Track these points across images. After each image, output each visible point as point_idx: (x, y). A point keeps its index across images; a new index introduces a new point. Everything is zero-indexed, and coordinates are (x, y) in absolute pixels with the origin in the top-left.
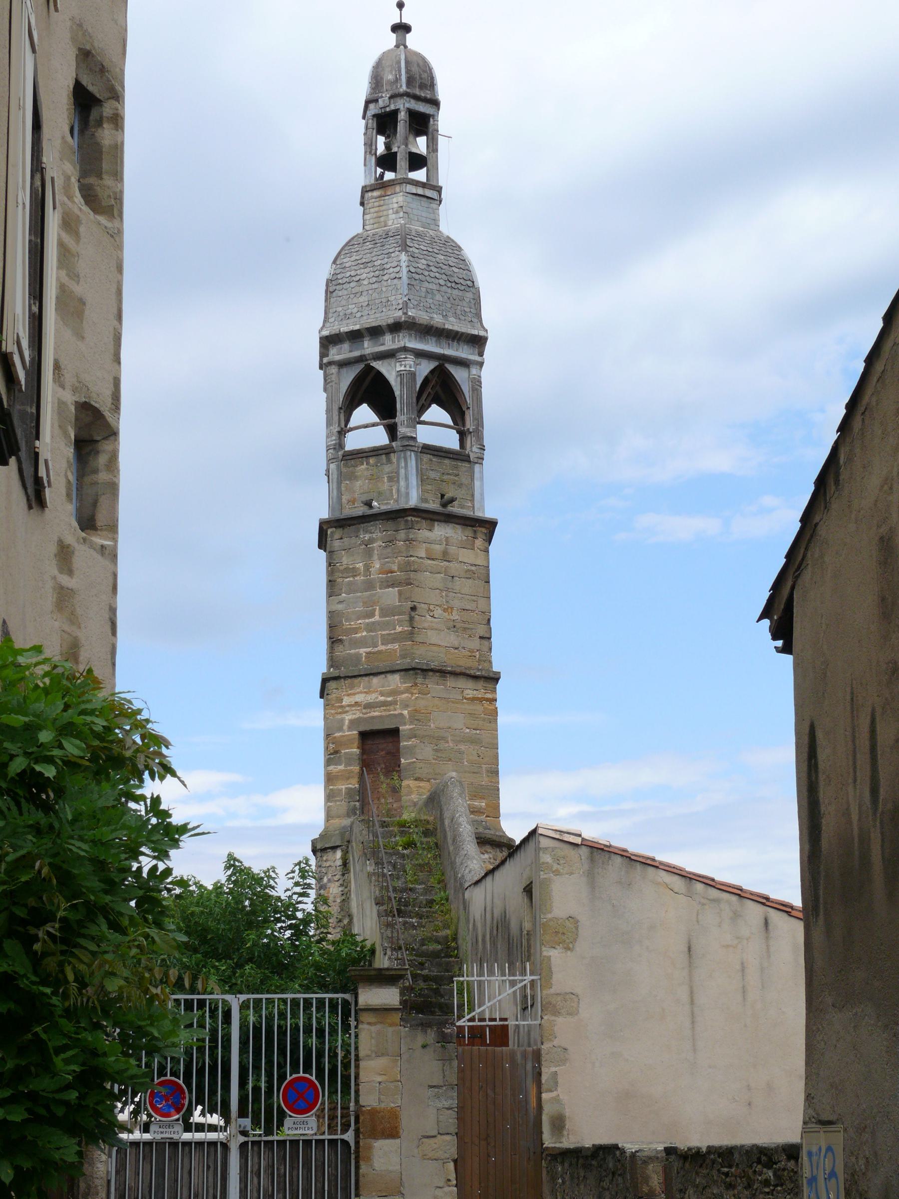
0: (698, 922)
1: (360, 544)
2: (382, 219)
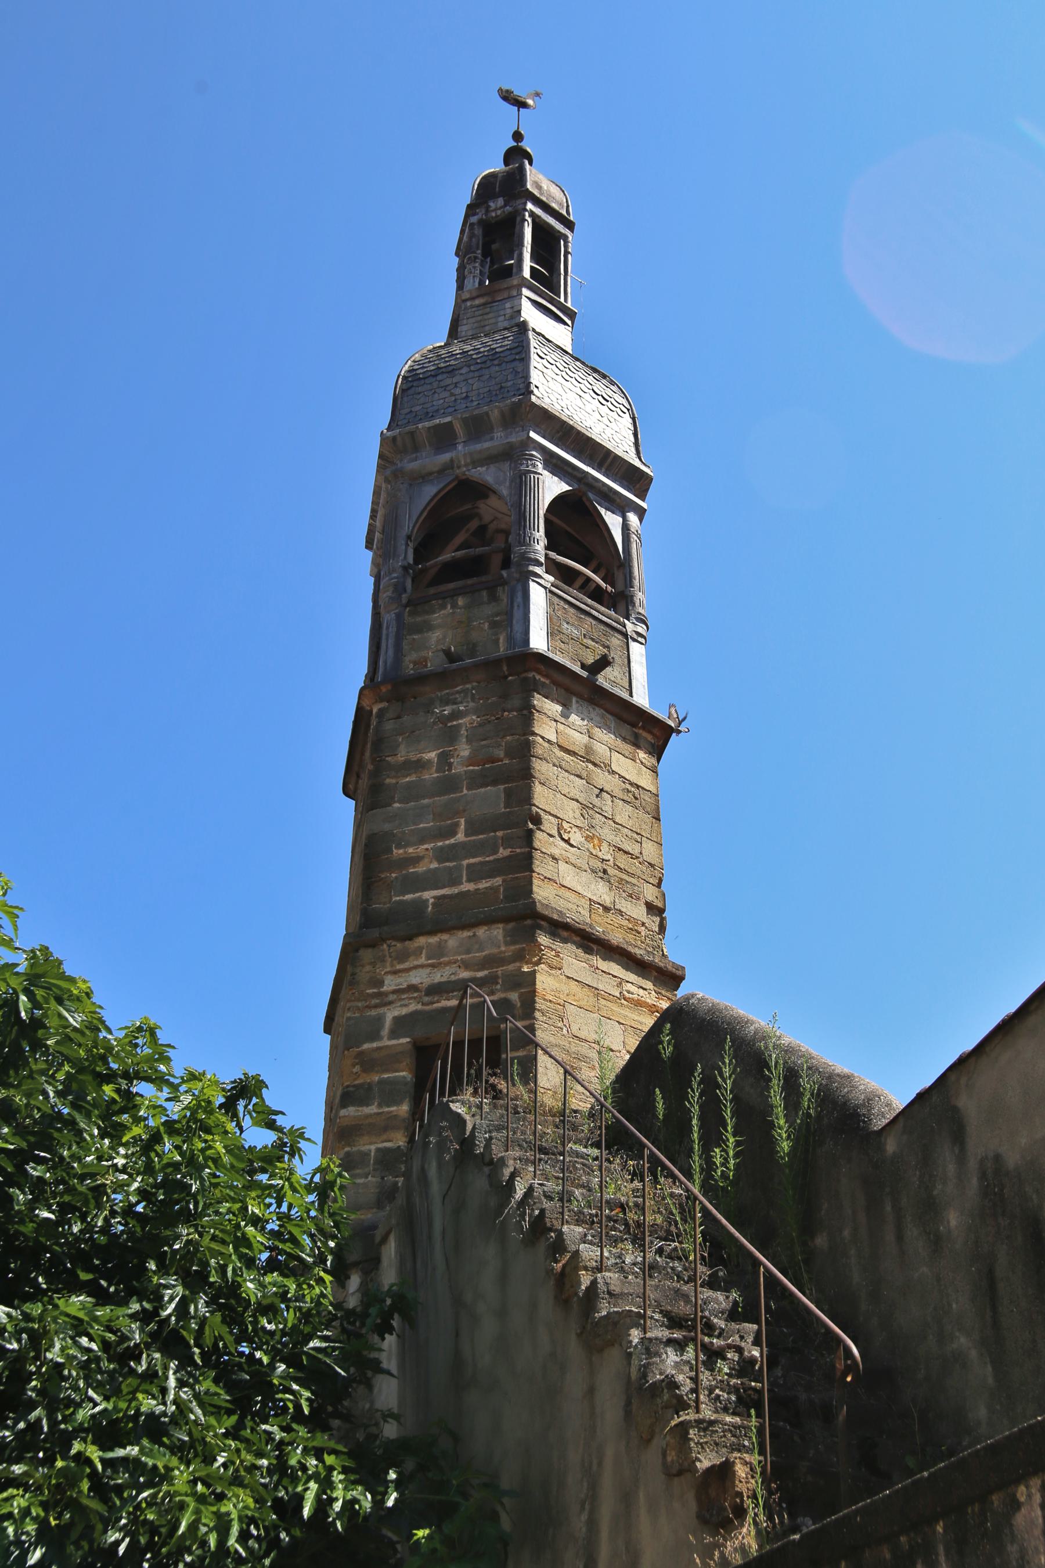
1: (434, 723)
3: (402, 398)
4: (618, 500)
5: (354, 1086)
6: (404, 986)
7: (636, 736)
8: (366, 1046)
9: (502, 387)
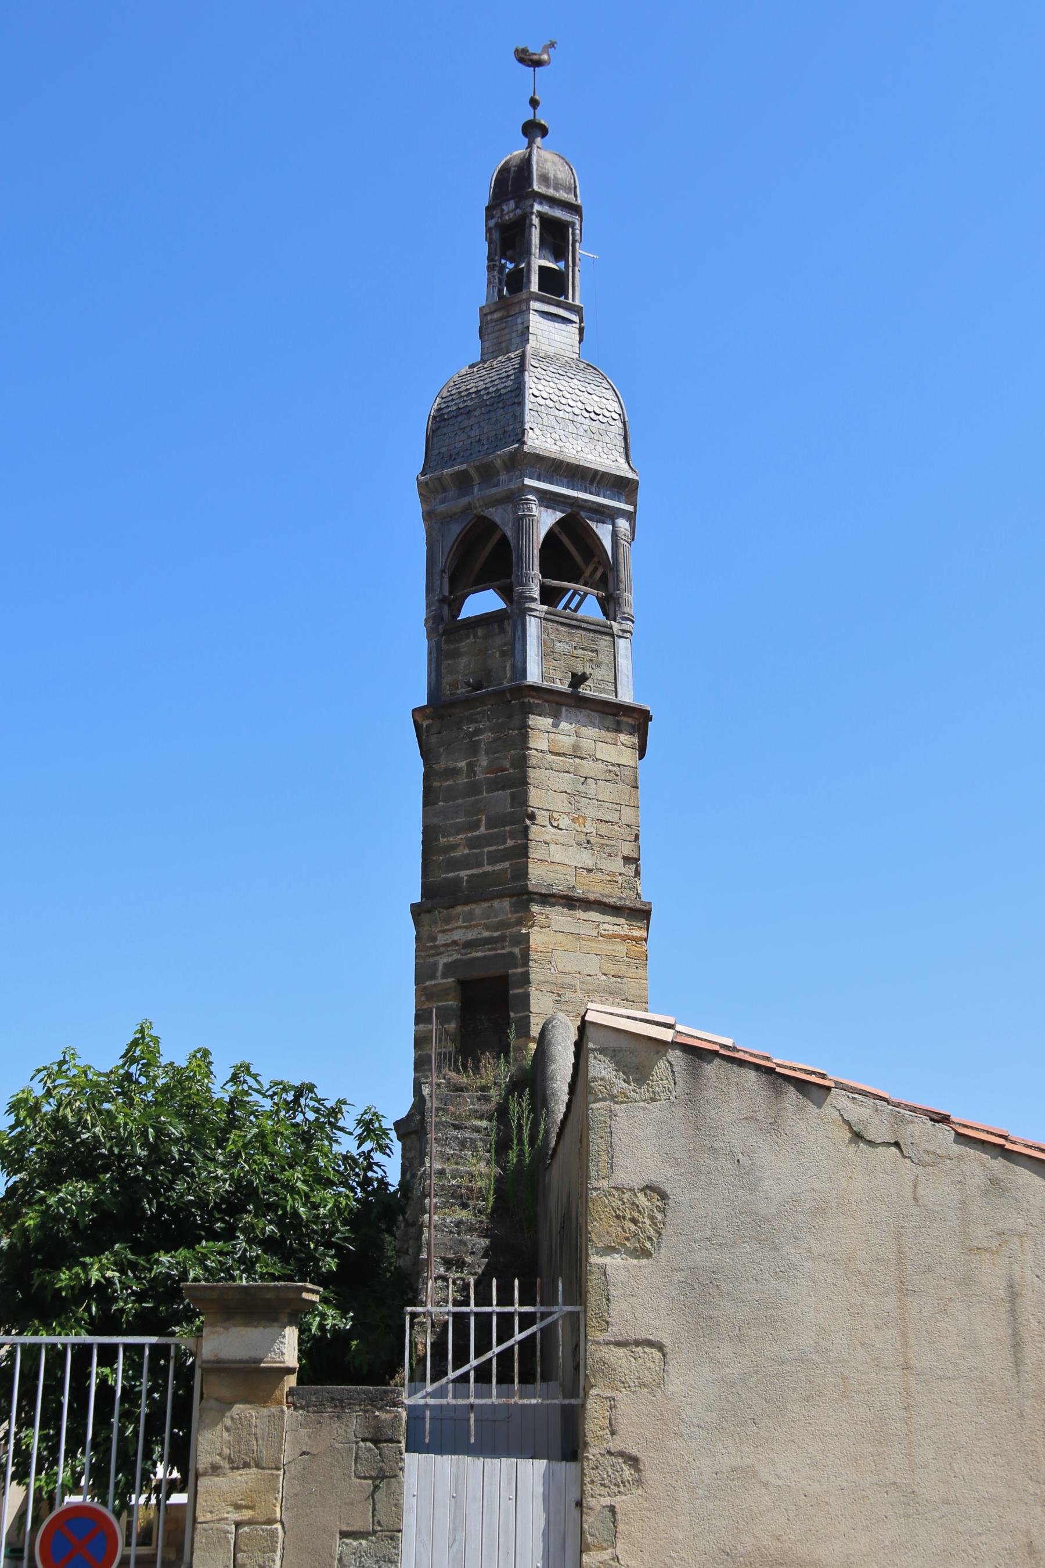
2: (504, 345)
3: (432, 438)
4: (607, 511)
5: (422, 1010)
6: (449, 941)
7: (618, 723)
8: (428, 983)
9: (505, 432)
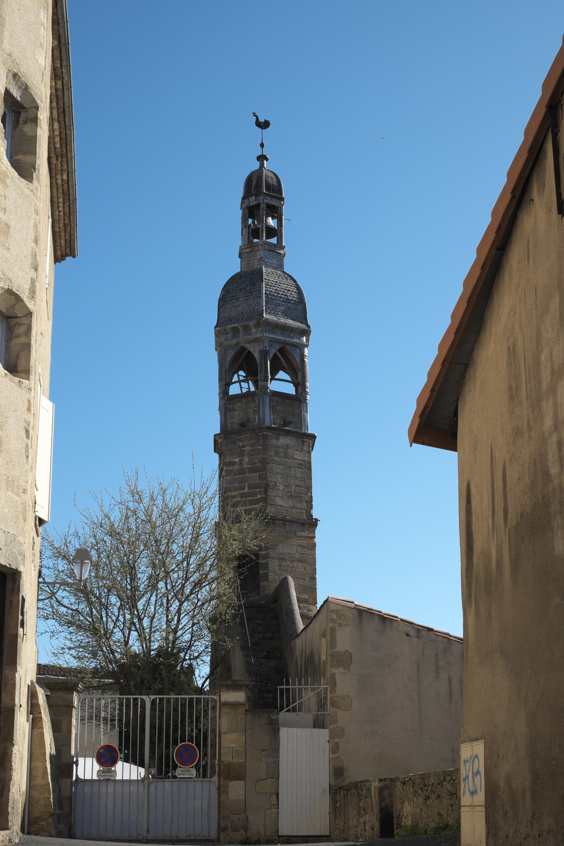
0: (423, 654)
2: (251, 264)
9: (254, 310)
